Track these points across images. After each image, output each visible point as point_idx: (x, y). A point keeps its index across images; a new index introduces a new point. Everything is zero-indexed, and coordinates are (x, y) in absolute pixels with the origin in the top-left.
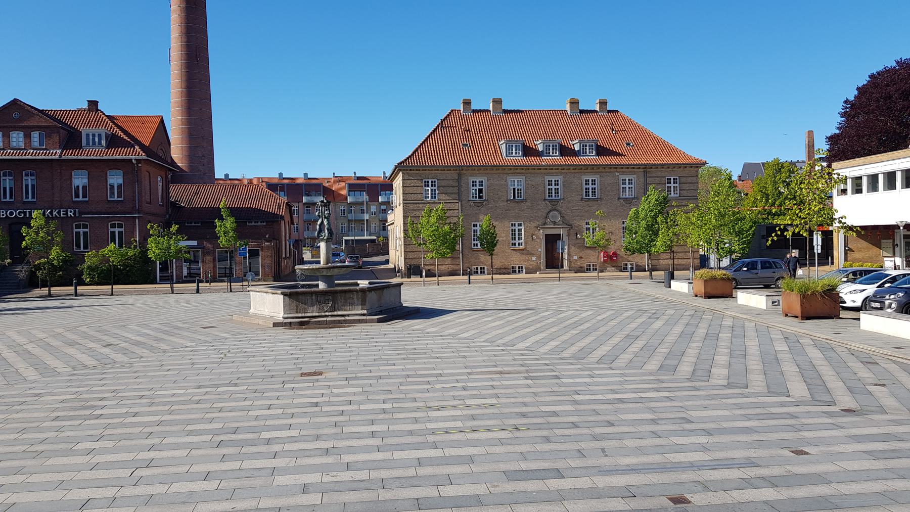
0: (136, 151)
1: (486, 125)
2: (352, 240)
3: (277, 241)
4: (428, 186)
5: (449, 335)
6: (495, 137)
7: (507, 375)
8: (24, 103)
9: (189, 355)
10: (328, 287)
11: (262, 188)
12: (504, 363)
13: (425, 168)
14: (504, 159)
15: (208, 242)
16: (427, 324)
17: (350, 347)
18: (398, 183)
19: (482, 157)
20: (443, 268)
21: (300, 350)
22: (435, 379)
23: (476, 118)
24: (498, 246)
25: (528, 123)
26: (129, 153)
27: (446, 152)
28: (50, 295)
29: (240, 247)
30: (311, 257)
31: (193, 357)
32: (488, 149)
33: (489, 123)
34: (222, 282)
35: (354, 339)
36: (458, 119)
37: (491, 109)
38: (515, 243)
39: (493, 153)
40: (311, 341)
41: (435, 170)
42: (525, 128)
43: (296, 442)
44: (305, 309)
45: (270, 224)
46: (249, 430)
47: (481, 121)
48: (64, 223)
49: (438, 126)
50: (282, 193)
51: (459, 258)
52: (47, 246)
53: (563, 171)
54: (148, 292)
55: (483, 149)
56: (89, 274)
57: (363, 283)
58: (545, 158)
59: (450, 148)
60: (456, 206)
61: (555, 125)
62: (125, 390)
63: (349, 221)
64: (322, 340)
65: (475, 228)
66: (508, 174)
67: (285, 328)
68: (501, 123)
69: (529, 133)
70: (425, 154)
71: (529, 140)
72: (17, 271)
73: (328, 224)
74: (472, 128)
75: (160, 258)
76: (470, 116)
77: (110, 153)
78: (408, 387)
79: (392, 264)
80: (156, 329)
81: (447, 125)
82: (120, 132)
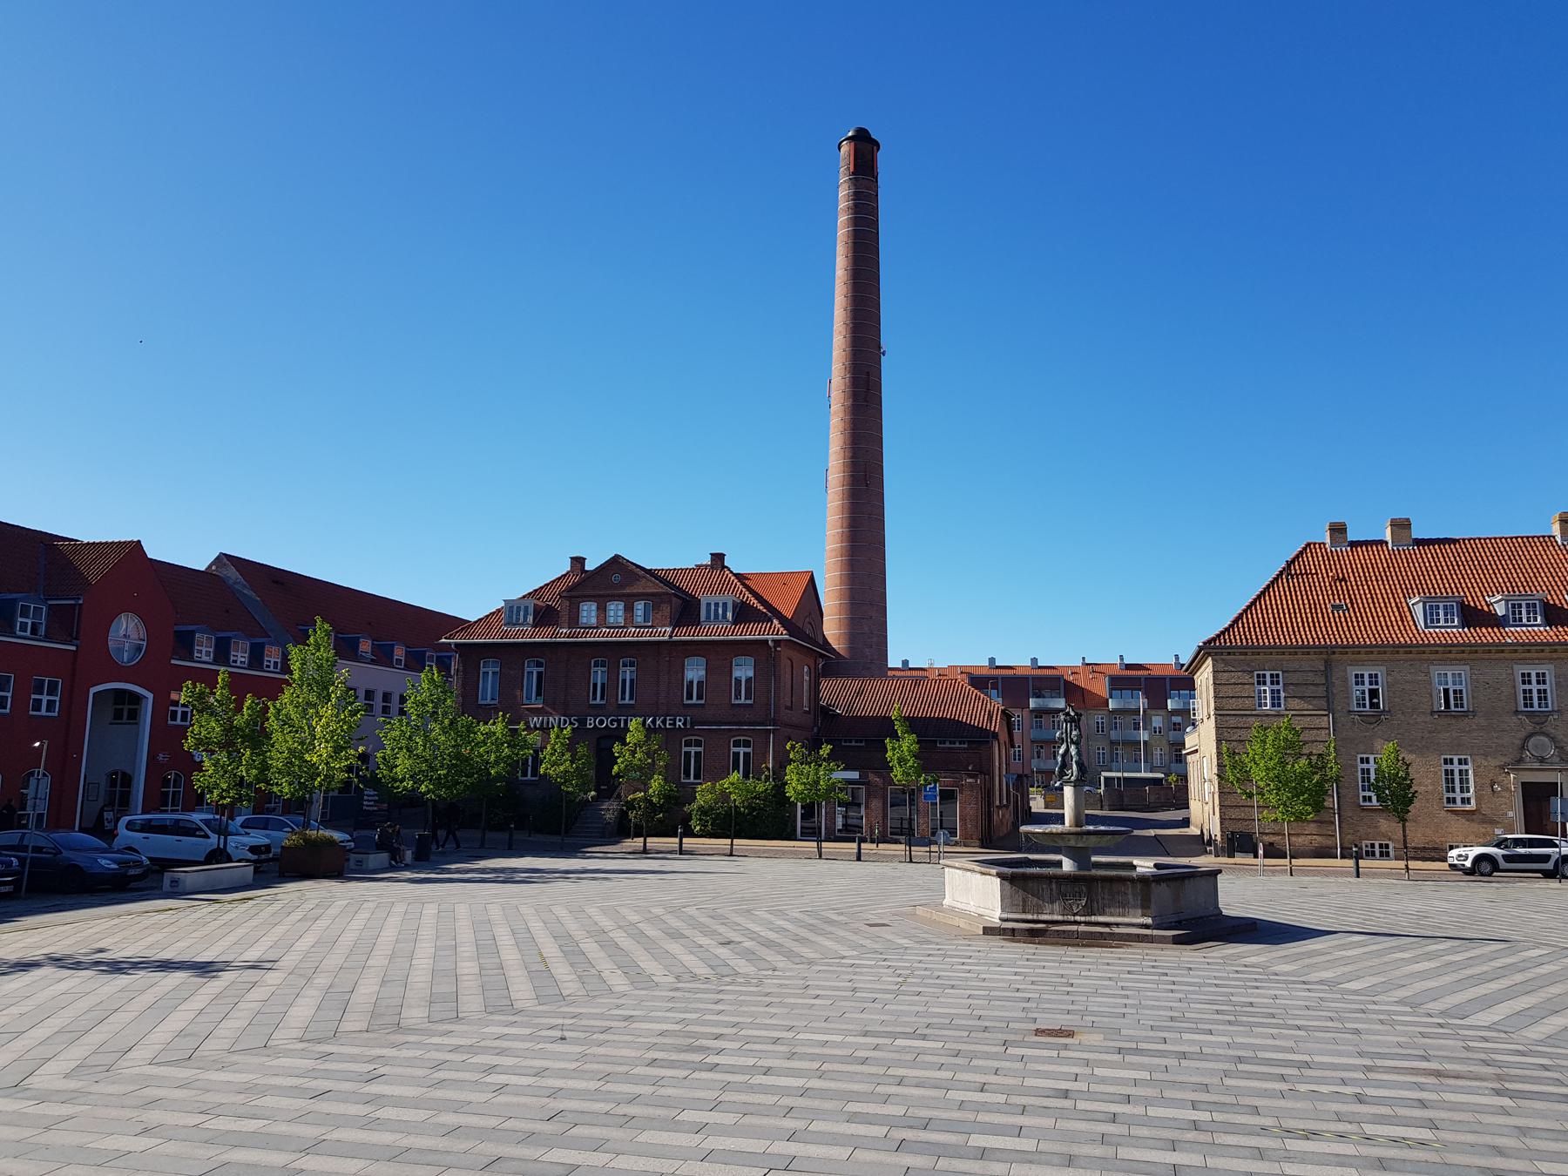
0: (775, 628)
1: (1378, 569)
2: (1119, 778)
3: (987, 777)
4: (1265, 683)
5: (1321, 982)
6: (1399, 591)
7: (1452, 1082)
8: (628, 561)
9: (848, 973)
10: (1080, 868)
11: (963, 685)
12: (1444, 1054)
13: (1257, 650)
14: (1421, 631)
15: (875, 773)
16: (1275, 955)
17: (1123, 988)
18: (1204, 677)
19: (1373, 628)
20: (1300, 840)
21: (1033, 983)
22: (1295, 1072)
23: (1359, 556)
24: (1416, 804)
25: (1471, 563)
26: (765, 631)
27: (1299, 620)
28: (645, 851)
29: (925, 786)
30: (1043, 806)
31: (855, 977)
32: (1386, 614)
33: (1385, 565)
34: (896, 843)
35: (1129, 972)
36: (1320, 559)
37: (1388, 538)
38: (1454, 799)
39: (1396, 621)
40: (1050, 968)
41: (1278, 654)
42: (1463, 572)
43: (1031, 1162)
44: (1038, 906)
45: (974, 746)
46: (950, 1126)
47: (1368, 561)
48: (671, 737)
49: (1281, 573)
50: (994, 692)
51: (1334, 823)
52: (647, 772)
53: (1554, 655)
54: (783, 852)
55: (1375, 614)
56: (700, 820)
57: (1145, 865)
58: (1512, 629)
59: (1306, 613)
60: (1323, 722)
61: (1530, 565)
62: (753, 1026)
63: (1112, 743)
64: (1072, 969)
65: (1365, 766)
66: (1431, 662)
67: (1004, 939)
68: (1411, 565)
69: (1473, 581)
70: (1257, 625)
71: (1474, 594)
72: (602, 810)
73: (1079, 753)
74: (1351, 575)
75: (802, 799)
76: (1345, 554)
77: (738, 632)
78: (1243, 1083)
79: (1196, 827)
80: (795, 921)
81: (1298, 572)
82: (752, 599)
